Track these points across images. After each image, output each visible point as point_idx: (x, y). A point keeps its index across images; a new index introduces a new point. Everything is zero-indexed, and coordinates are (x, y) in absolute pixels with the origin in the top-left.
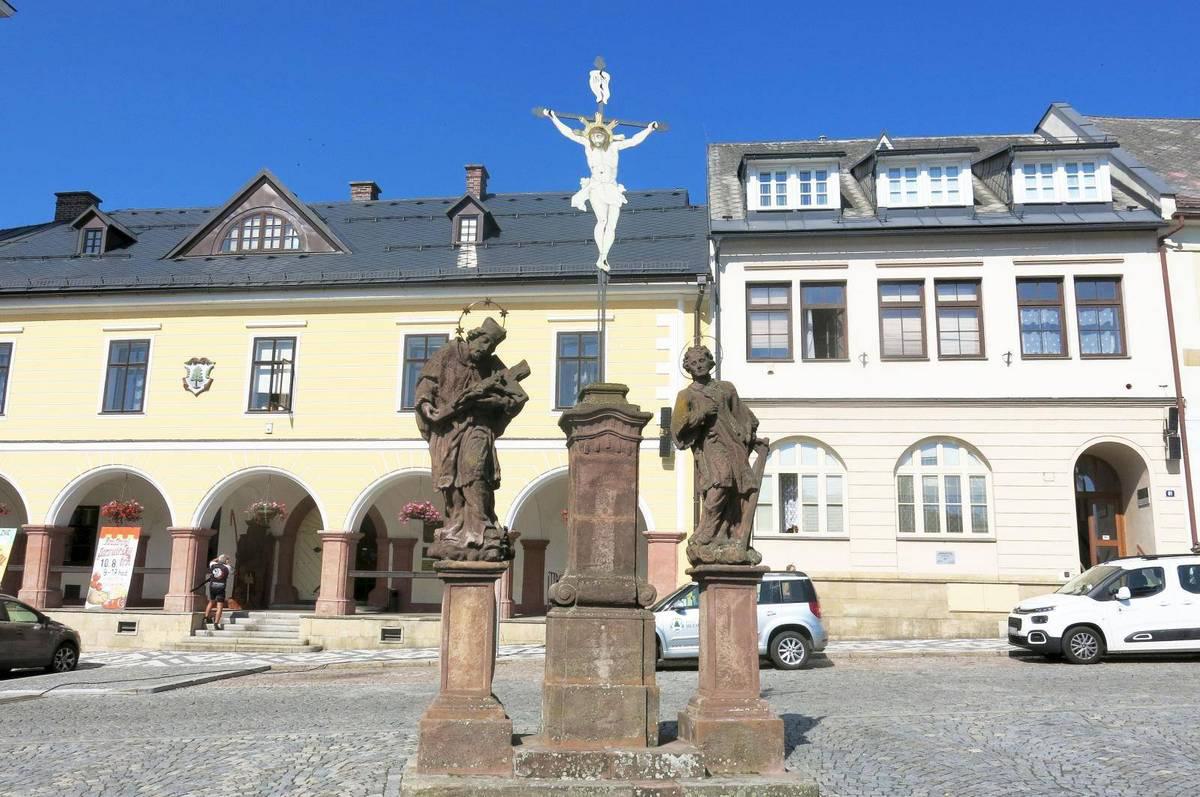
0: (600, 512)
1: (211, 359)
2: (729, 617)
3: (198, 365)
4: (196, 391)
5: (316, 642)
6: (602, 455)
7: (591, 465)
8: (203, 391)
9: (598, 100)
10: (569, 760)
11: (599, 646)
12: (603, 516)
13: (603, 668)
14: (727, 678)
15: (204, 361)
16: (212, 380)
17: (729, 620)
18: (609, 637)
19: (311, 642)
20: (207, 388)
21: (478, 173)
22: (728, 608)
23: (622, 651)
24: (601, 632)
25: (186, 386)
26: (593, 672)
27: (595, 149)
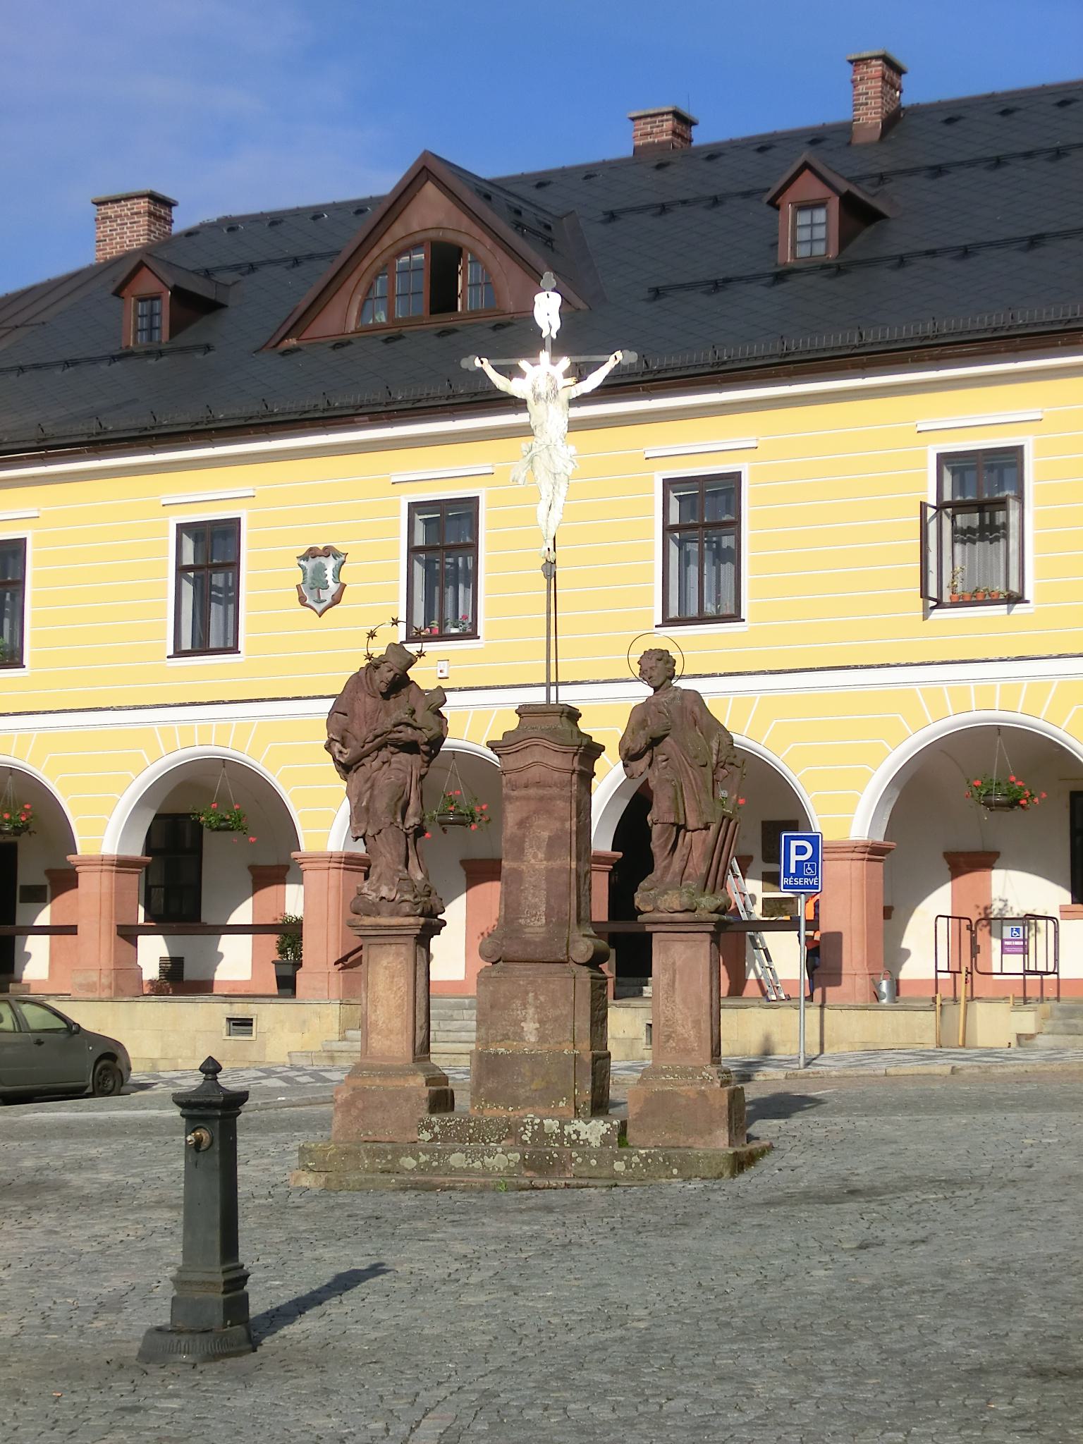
0: (530, 857)
3: (318, 559)
4: (319, 607)
6: (532, 791)
7: (518, 803)
8: (330, 606)
9: (544, 335)
10: (472, 1124)
11: (524, 1006)
12: (533, 861)
13: (530, 1028)
14: (672, 1044)
15: (328, 552)
16: (343, 586)
17: (674, 977)
18: (536, 998)
20: (336, 600)
21: (877, 68)
22: (674, 963)
23: (552, 1013)
24: (527, 993)
25: (302, 600)
26: (519, 1036)
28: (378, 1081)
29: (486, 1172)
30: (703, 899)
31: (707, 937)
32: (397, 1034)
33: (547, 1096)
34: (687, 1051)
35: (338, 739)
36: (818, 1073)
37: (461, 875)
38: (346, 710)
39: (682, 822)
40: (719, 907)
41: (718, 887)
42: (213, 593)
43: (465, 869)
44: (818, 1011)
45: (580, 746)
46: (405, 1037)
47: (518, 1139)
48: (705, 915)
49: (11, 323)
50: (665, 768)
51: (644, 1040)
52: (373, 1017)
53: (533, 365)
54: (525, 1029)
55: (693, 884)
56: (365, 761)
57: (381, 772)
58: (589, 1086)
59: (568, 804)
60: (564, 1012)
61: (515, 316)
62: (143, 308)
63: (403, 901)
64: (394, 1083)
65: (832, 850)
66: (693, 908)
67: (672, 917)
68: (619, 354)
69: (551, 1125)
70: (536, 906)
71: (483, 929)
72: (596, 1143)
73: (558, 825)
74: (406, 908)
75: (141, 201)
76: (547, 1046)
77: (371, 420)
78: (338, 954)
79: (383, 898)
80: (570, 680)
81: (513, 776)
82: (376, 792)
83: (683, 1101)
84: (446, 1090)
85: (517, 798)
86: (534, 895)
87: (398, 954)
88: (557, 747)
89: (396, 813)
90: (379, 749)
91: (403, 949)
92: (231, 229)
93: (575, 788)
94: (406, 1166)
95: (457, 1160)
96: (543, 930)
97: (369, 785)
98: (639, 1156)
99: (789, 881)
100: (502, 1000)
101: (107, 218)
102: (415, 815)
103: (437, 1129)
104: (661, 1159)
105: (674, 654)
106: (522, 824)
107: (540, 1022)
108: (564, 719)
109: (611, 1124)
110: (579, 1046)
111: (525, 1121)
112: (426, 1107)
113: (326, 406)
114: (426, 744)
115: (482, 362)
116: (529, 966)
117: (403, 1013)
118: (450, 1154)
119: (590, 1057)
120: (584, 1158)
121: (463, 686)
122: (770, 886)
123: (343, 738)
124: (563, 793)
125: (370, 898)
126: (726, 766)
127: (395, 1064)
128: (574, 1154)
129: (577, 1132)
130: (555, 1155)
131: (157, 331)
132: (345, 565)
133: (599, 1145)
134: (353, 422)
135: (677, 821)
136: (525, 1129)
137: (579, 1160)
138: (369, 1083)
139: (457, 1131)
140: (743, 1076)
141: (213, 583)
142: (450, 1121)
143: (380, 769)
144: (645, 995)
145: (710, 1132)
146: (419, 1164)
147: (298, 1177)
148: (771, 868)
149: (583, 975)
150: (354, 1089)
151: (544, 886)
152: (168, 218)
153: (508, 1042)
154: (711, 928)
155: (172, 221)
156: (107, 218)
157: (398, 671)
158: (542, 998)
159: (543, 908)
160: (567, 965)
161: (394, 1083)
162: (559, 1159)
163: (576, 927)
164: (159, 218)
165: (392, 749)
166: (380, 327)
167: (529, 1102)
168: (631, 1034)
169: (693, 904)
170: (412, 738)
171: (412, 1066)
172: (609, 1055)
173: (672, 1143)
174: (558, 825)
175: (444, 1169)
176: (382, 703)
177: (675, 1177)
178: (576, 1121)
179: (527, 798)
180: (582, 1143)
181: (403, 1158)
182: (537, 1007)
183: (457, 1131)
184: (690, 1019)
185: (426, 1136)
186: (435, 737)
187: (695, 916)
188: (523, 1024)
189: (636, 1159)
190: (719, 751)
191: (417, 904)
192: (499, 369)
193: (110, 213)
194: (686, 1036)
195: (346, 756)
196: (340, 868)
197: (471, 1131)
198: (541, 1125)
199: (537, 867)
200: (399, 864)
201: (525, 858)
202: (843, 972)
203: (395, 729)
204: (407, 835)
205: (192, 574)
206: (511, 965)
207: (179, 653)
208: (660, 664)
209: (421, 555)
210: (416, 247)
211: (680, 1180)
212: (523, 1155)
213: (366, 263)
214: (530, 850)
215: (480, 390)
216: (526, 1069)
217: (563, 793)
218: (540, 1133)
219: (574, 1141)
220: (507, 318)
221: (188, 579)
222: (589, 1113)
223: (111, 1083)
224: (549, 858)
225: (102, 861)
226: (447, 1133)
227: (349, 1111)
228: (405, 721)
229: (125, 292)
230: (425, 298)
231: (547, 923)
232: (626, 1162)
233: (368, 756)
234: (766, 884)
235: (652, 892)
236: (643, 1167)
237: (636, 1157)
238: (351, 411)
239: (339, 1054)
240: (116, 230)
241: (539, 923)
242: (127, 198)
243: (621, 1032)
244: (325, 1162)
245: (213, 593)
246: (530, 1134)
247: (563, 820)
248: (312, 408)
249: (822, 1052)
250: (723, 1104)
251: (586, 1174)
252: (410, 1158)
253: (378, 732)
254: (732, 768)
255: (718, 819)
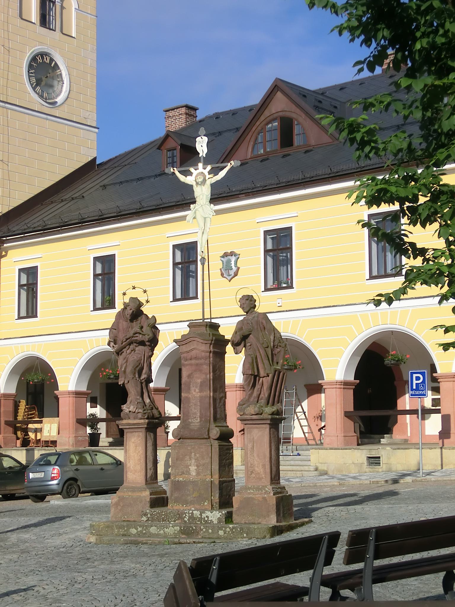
0: (193, 391)
1: (237, 251)
2: (254, 443)
4: (229, 278)
5: (323, 468)
6: (193, 362)
7: (187, 367)
10: (163, 513)
12: (194, 393)
13: (193, 469)
14: (253, 475)
15: (232, 254)
16: (239, 268)
17: (254, 445)
18: (195, 455)
19: (320, 468)
20: (236, 274)
22: (253, 438)
23: (202, 462)
24: (191, 453)
25: (222, 275)
26: (188, 472)
27: (199, 186)
28: (130, 494)
29: (165, 536)
30: (267, 409)
31: (268, 426)
32: (139, 472)
33: (200, 499)
34: (260, 479)
35: (112, 341)
36: (426, 479)
37: (304, 391)
38: (116, 328)
39: (256, 374)
40: (274, 412)
41: (276, 403)
42: (191, 274)
43: (306, 388)
44: (440, 450)
45: (212, 340)
46: (142, 473)
47: (183, 520)
48: (264, 416)
49: (123, 164)
50: (250, 349)
51: (366, 464)
52: (129, 465)
53: (196, 170)
54: (191, 469)
55: (263, 402)
56: (124, 350)
57: (131, 355)
58: (218, 495)
59: (208, 367)
60: (207, 462)
61: (315, 146)
62: (169, 154)
63: (138, 413)
64: (136, 494)
65: (445, 377)
66: (260, 413)
67: (251, 417)
68: (232, 162)
69: (197, 513)
70: (195, 413)
71: (315, 415)
72: (215, 522)
73: (204, 376)
74: (140, 415)
75: (183, 109)
76: (200, 477)
77: (245, 196)
78: (241, 427)
79: (130, 411)
80: (332, 305)
81: (185, 355)
82: (128, 364)
83: (256, 502)
84: (163, 498)
85: (187, 365)
86: (195, 408)
87: (139, 436)
88: (202, 341)
89: (135, 373)
90: (130, 344)
91: (141, 434)
92: (217, 118)
93: (211, 359)
94: (132, 533)
95: (153, 530)
96: (199, 424)
97: (125, 361)
98: (230, 528)
99: (413, 392)
100: (181, 456)
101: (170, 117)
102: (145, 374)
103: (149, 516)
104: (239, 529)
105: (255, 297)
106: (189, 376)
107: (197, 466)
108: (208, 328)
109: (222, 513)
110: (214, 477)
111: (186, 512)
112: (148, 505)
113: (229, 191)
114: (148, 341)
115: (174, 170)
116: (193, 441)
117: (141, 463)
118: (150, 527)
119: (218, 482)
120: (206, 529)
121: (288, 309)
122: (435, 393)
123: (115, 340)
124: (206, 362)
125: (126, 411)
126: (278, 347)
127: (138, 485)
128: (202, 527)
129: (207, 517)
130: (194, 528)
131: (175, 163)
132: (239, 259)
133: (217, 523)
134: (239, 197)
135: (253, 373)
136: (186, 516)
137: (204, 530)
138: (126, 494)
139: (157, 516)
140: (394, 481)
141: (191, 269)
142: (154, 512)
143: (130, 353)
144: (382, 443)
145: (268, 516)
146: (138, 532)
147: (89, 538)
148: (435, 385)
149: (215, 444)
150: (119, 497)
151: (199, 404)
152: (195, 115)
153: (184, 475)
154: (269, 422)
155: (197, 116)
156: (170, 117)
157: (134, 310)
158: (198, 455)
159: (199, 415)
160: (209, 440)
161: (136, 494)
162: (196, 529)
163: (213, 423)
164: (191, 115)
165: (135, 344)
166: (261, 155)
167: (192, 503)
168: (360, 461)
169: (260, 411)
170: (142, 339)
171: (145, 486)
172: (234, 480)
173: (252, 521)
174: (204, 376)
175: (148, 534)
176: (130, 324)
177: (245, 538)
178: (207, 512)
179: (191, 365)
180: (209, 522)
181: (131, 529)
182: (196, 459)
183: (157, 516)
184: (261, 464)
185: (144, 519)
186: (151, 338)
187: (261, 416)
188: (190, 467)
189: (228, 529)
190: (274, 340)
191: (145, 413)
192: (183, 173)
193: (171, 115)
194: (259, 472)
195: (115, 348)
196: (241, 390)
197: (163, 516)
198: (192, 513)
199: (196, 395)
200: (138, 396)
201: (191, 392)
202: (451, 432)
203: (135, 336)
204: (142, 383)
205: (180, 266)
206: (185, 440)
207: (175, 300)
208: (247, 302)
209: (271, 253)
210: (274, 120)
211: (247, 539)
212: (181, 528)
213: (254, 129)
214: (193, 388)
215: (290, 180)
216: (190, 487)
217: (206, 362)
218: (192, 517)
219: (206, 521)
220: (311, 148)
221: (179, 268)
222: (218, 508)
223: (74, 491)
224: (201, 391)
225: (69, 393)
226: (153, 517)
227: (117, 507)
228: (138, 332)
229: (162, 148)
230: (278, 143)
231: (200, 421)
232: (224, 530)
233: (125, 348)
234: (433, 392)
235: (244, 406)
236: (232, 533)
237: (228, 529)
238: (238, 193)
239: (239, 471)
240: (173, 122)
241: (197, 421)
242: (177, 108)
243: (356, 460)
244: (99, 531)
245: (191, 274)
246: (188, 518)
247: (206, 374)
248: (223, 192)
249: (442, 468)
250: (273, 503)
251: (207, 537)
252: (134, 529)
253: (128, 337)
254: (281, 348)
255: (273, 372)
